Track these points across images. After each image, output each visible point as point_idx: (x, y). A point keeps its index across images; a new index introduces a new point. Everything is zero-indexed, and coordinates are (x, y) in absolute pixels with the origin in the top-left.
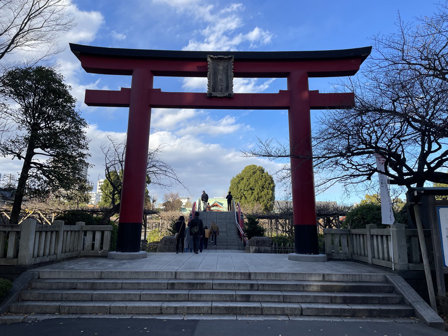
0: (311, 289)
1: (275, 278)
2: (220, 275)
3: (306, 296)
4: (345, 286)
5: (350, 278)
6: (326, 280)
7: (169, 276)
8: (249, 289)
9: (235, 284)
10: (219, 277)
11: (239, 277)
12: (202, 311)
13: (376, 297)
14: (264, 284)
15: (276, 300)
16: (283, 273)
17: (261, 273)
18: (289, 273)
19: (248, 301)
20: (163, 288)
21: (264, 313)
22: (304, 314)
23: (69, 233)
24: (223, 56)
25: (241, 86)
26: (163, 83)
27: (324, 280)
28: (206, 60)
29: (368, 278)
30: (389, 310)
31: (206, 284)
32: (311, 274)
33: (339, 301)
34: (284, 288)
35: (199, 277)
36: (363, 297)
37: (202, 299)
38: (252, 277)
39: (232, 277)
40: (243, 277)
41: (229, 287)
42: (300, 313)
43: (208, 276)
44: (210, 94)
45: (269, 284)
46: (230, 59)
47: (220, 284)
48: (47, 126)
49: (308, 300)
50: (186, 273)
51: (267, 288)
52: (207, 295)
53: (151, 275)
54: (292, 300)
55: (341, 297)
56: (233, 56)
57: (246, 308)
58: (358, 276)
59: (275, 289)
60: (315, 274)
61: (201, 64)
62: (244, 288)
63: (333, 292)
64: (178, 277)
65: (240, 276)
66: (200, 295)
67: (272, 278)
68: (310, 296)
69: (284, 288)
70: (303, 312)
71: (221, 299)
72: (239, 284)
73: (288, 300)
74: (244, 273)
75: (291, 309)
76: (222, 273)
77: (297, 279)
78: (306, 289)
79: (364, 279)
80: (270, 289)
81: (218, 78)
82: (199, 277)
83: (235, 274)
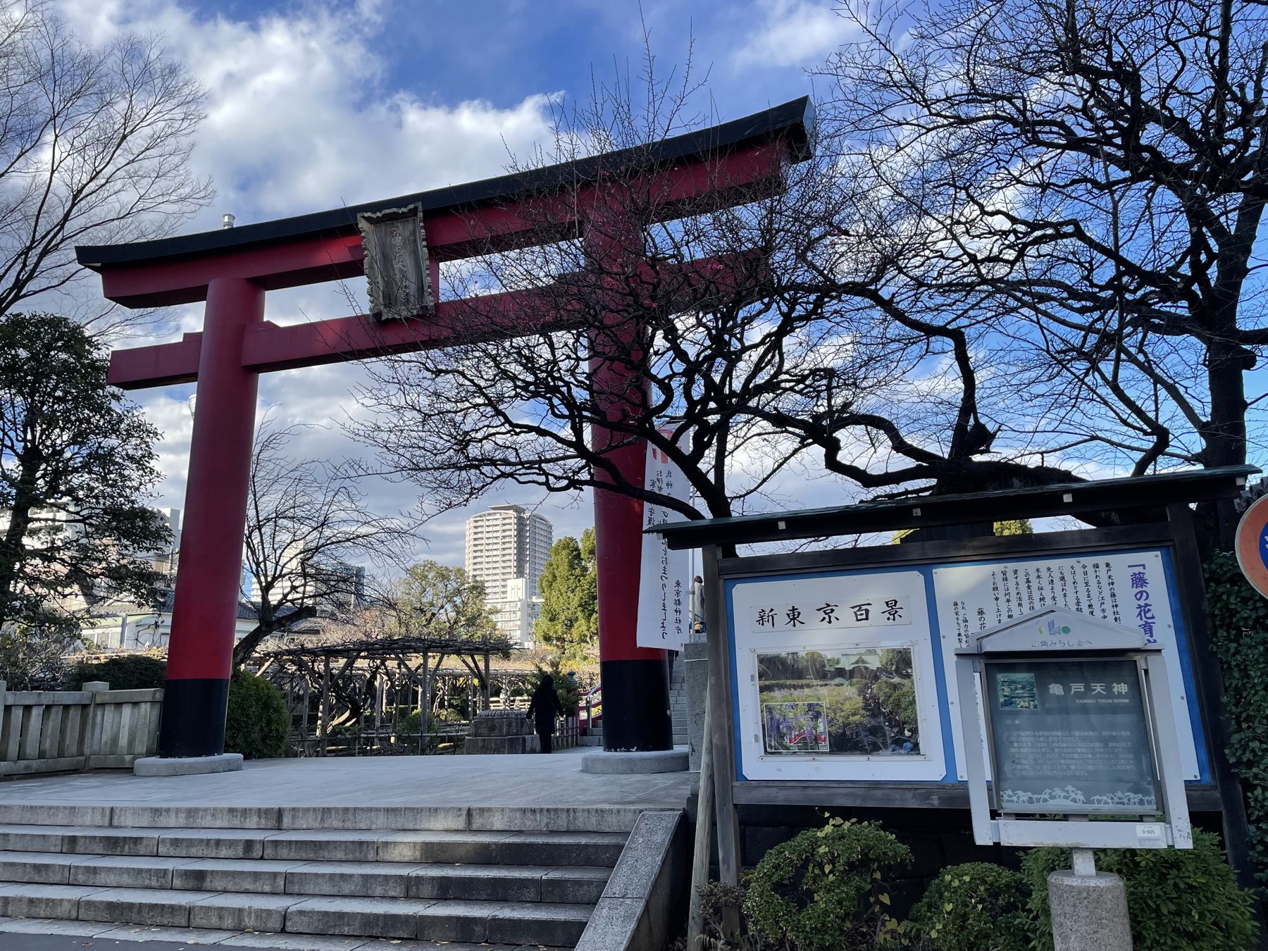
0: (395, 854)
1: (341, 825)
2: (209, 818)
3: (342, 876)
4: (488, 845)
5: (542, 822)
6: (475, 827)
7: (98, 820)
8: (241, 855)
9: (209, 841)
10: (208, 821)
11: (253, 821)
12: (60, 911)
13: (532, 881)
14: (276, 842)
15: (267, 888)
16: (362, 809)
17: (308, 810)
18: (378, 810)
19: (199, 889)
20: (52, 849)
21: (194, 923)
22: (288, 929)
23: (36, 712)
24: (394, 210)
25: (464, 278)
26: (286, 309)
27: (469, 830)
28: (352, 230)
29: (594, 820)
30: (520, 921)
31: (145, 842)
32: (436, 810)
33: (426, 891)
34: (326, 854)
35: (163, 821)
36: (495, 879)
37: (102, 878)
38: (286, 821)
39: (236, 823)
40: (263, 821)
41: (193, 851)
42: (278, 926)
43: (182, 821)
44: (377, 315)
45: (290, 842)
46: (414, 212)
47: (176, 842)
48: (532, 388)
49: (347, 888)
50: (135, 811)
51: (284, 853)
52: (110, 870)
53: (61, 815)
54: (310, 889)
55: (433, 878)
56: (420, 205)
57: (153, 907)
58: (564, 815)
59: (304, 857)
60: (447, 810)
61: (350, 241)
62: (230, 853)
63: (449, 863)
64: (115, 822)
65: (255, 819)
66: (95, 870)
67: (335, 824)
68: (351, 876)
69: (326, 854)
70: (288, 923)
71: (139, 882)
72: (218, 843)
73: (296, 889)
74: (267, 811)
75: (260, 913)
76: (215, 812)
77: (399, 826)
78: (383, 855)
79: (581, 823)
80: (293, 855)
81: (394, 270)
82: (163, 821)
83: (245, 812)
